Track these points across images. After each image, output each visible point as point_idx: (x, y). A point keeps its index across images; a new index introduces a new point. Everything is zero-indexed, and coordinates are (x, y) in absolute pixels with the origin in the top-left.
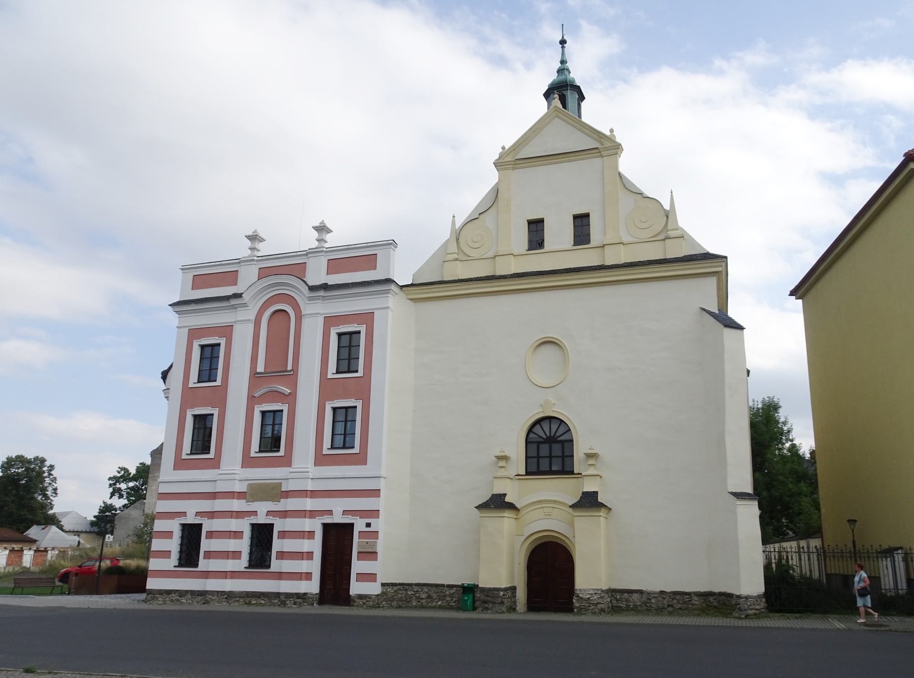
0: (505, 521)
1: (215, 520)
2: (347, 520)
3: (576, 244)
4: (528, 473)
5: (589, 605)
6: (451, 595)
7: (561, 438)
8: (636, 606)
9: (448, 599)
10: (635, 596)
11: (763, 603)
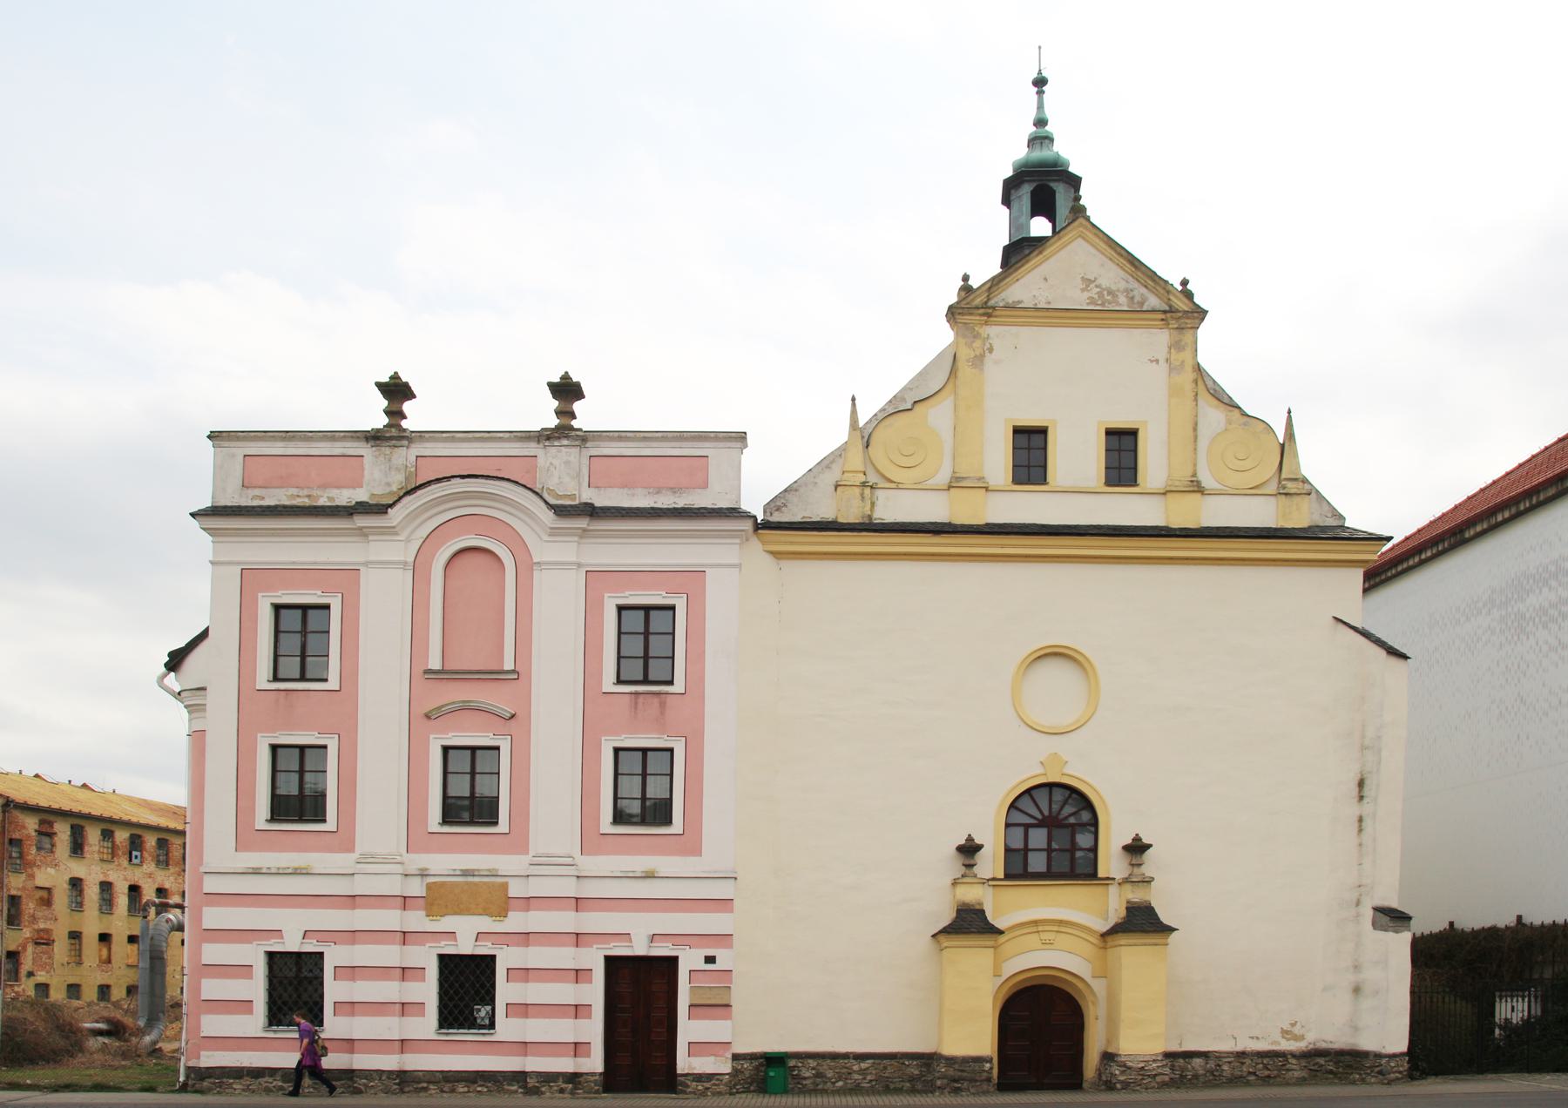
0: (973, 958)
1: (357, 947)
2: (310, 947)
3: (1109, 483)
4: (1008, 876)
5: (1139, 1078)
6: (863, 1072)
7: (1072, 820)
8: (1196, 1076)
9: (856, 1076)
10: (1197, 1062)
11: (1405, 1065)
